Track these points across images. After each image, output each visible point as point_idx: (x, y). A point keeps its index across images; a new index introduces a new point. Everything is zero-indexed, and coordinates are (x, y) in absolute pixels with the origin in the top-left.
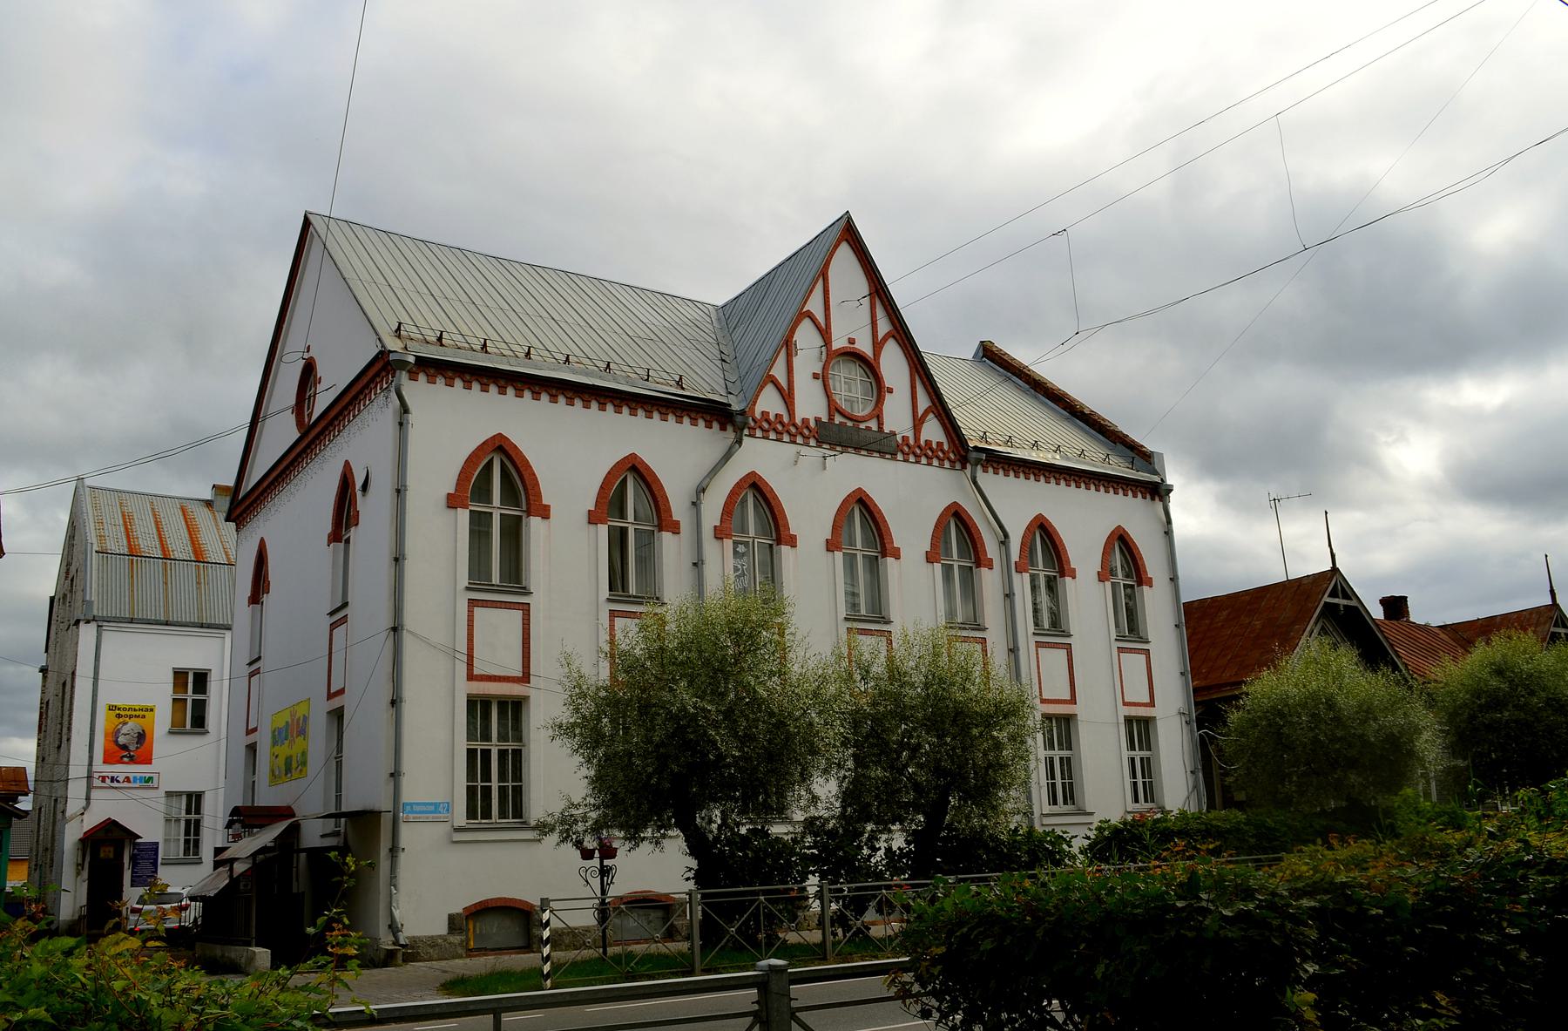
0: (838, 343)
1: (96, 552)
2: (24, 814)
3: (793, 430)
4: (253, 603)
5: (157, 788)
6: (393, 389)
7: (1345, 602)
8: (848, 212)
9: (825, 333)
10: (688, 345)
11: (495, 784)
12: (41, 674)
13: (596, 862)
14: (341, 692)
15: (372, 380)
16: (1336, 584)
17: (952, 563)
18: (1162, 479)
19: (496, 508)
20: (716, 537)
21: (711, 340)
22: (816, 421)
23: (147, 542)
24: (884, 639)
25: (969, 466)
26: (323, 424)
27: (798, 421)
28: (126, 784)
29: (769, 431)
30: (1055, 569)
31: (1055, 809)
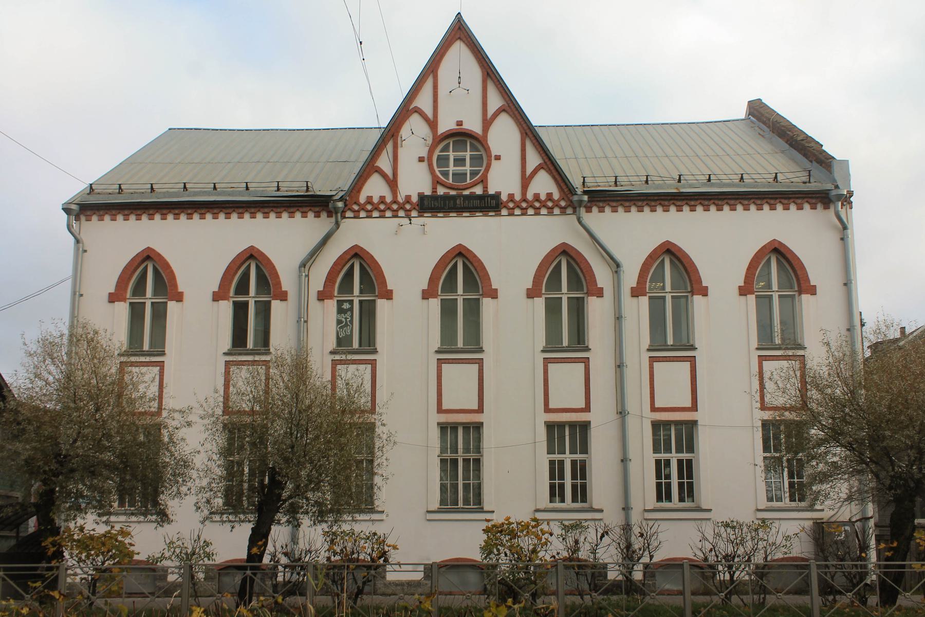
8: (459, 13)
9: (432, 124)
19: (565, 294)
20: (318, 300)
24: (370, 366)
29: (553, 208)
30: (686, 288)
31: (793, 504)
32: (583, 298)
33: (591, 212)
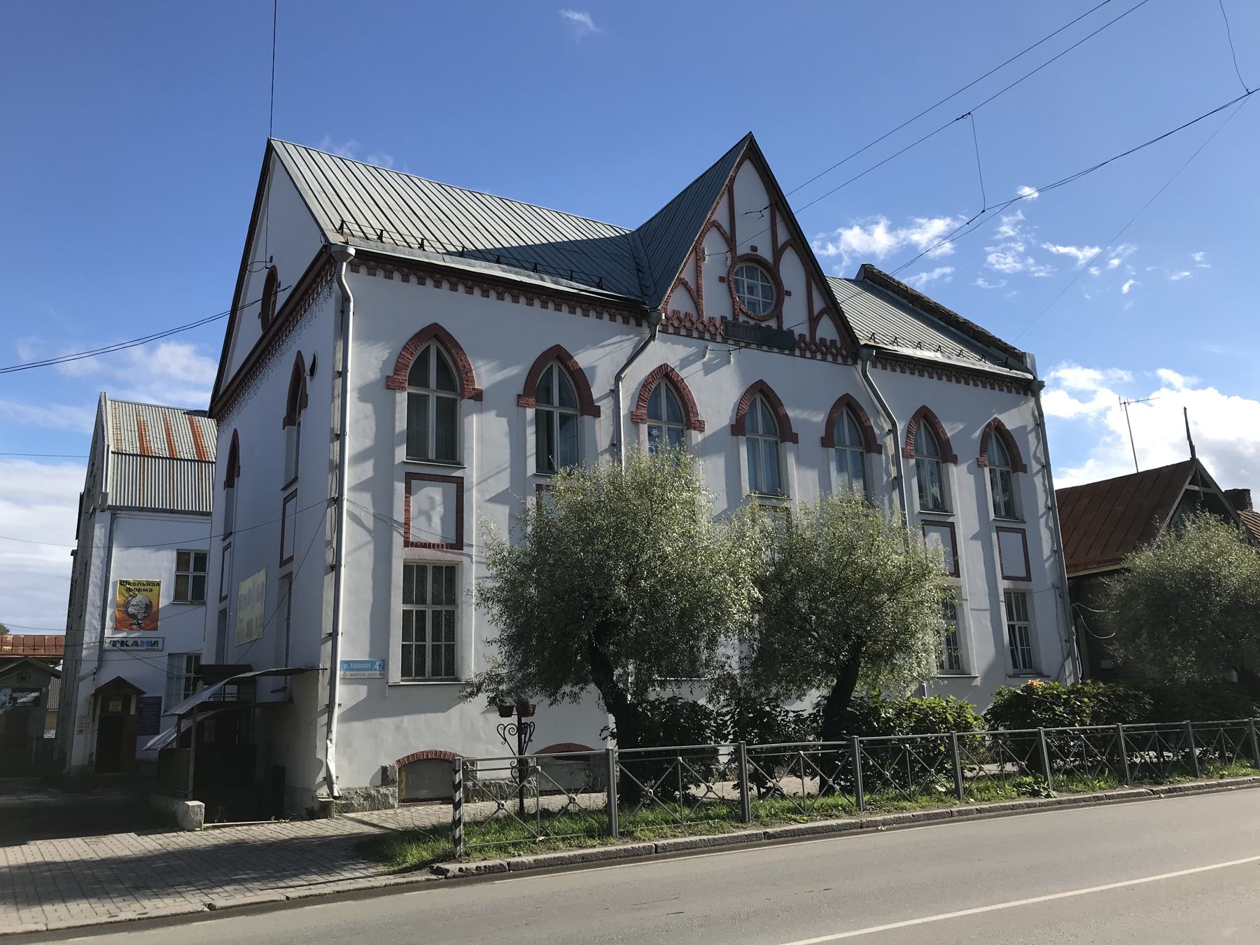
0: (743, 249)
1: (112, 452)
2: (57, 675)
3: (701, 327)
4: (227, 487)
5: (162, 651)
6: (335, 280)
7: (1206, 490)
8: (751, 132)
9: (731, 241)
10: (608, 257)
11: (429, 643)
12: (72, 557)
13: (514, 719)
14: (291, 559)
15: (318, 275)
16: (1196, 473)
17: (845, 448)
18: (1034, 377)
21: (628, 255)
22: (722, 320)
23: (158, 446)
25: (860, 362)
26: (280, 320)
27: (705, 319)
28: (134, 648)
32: (455, 400)
33: (472, 294)
